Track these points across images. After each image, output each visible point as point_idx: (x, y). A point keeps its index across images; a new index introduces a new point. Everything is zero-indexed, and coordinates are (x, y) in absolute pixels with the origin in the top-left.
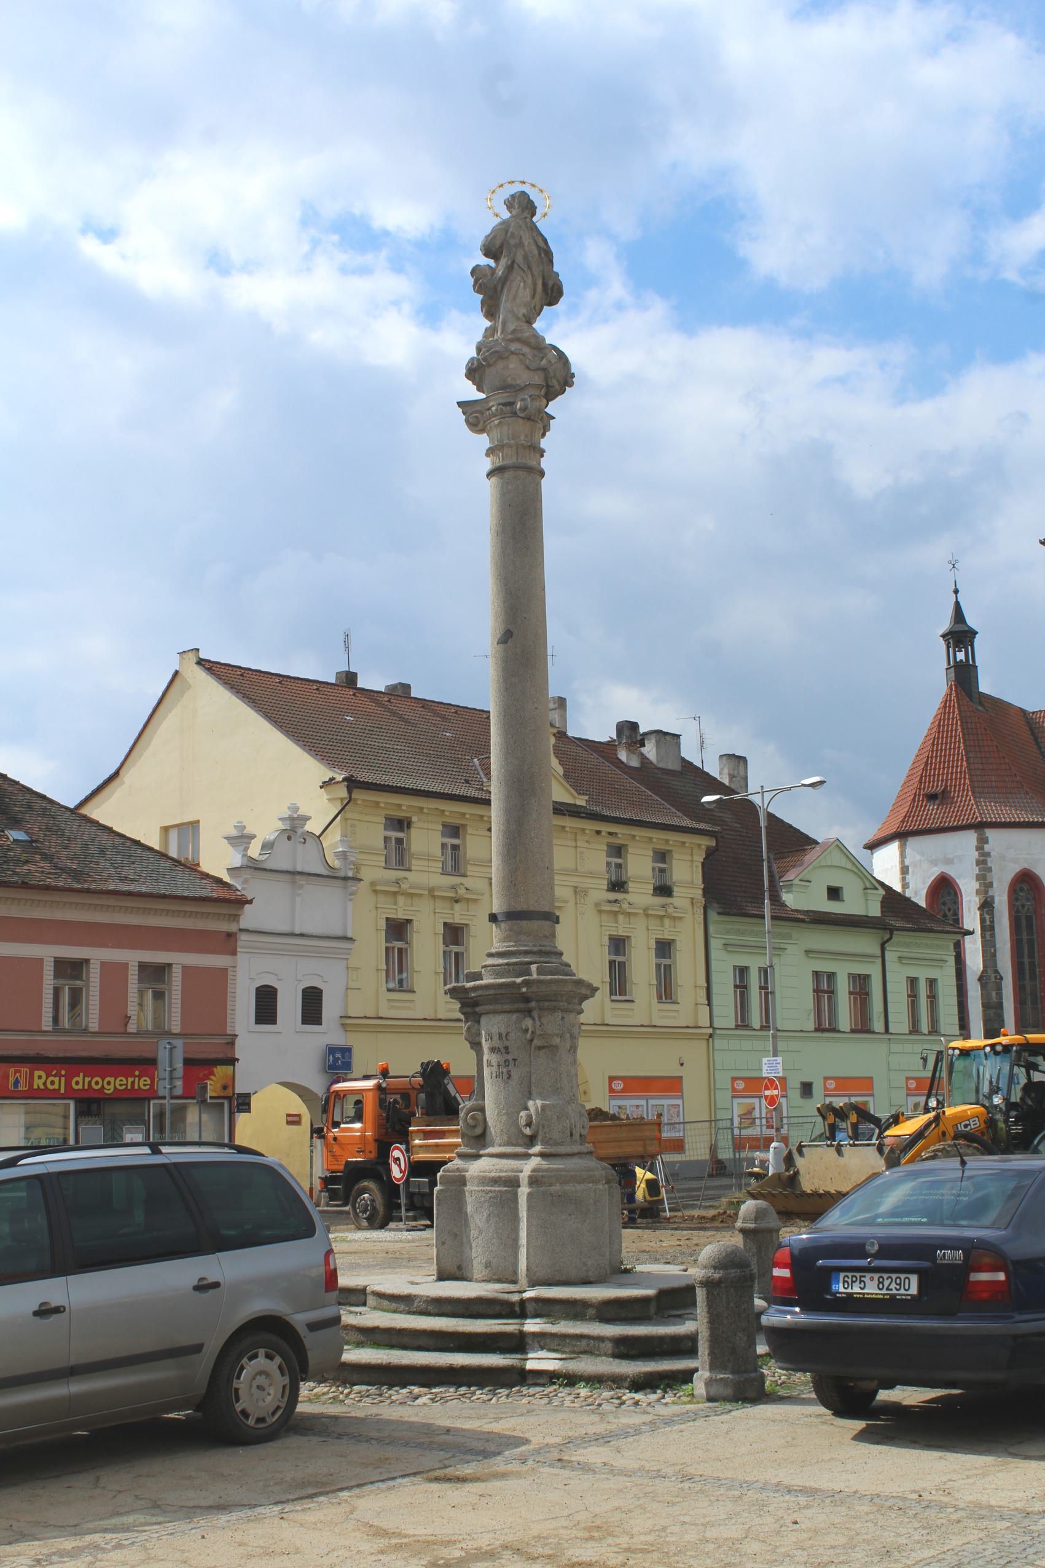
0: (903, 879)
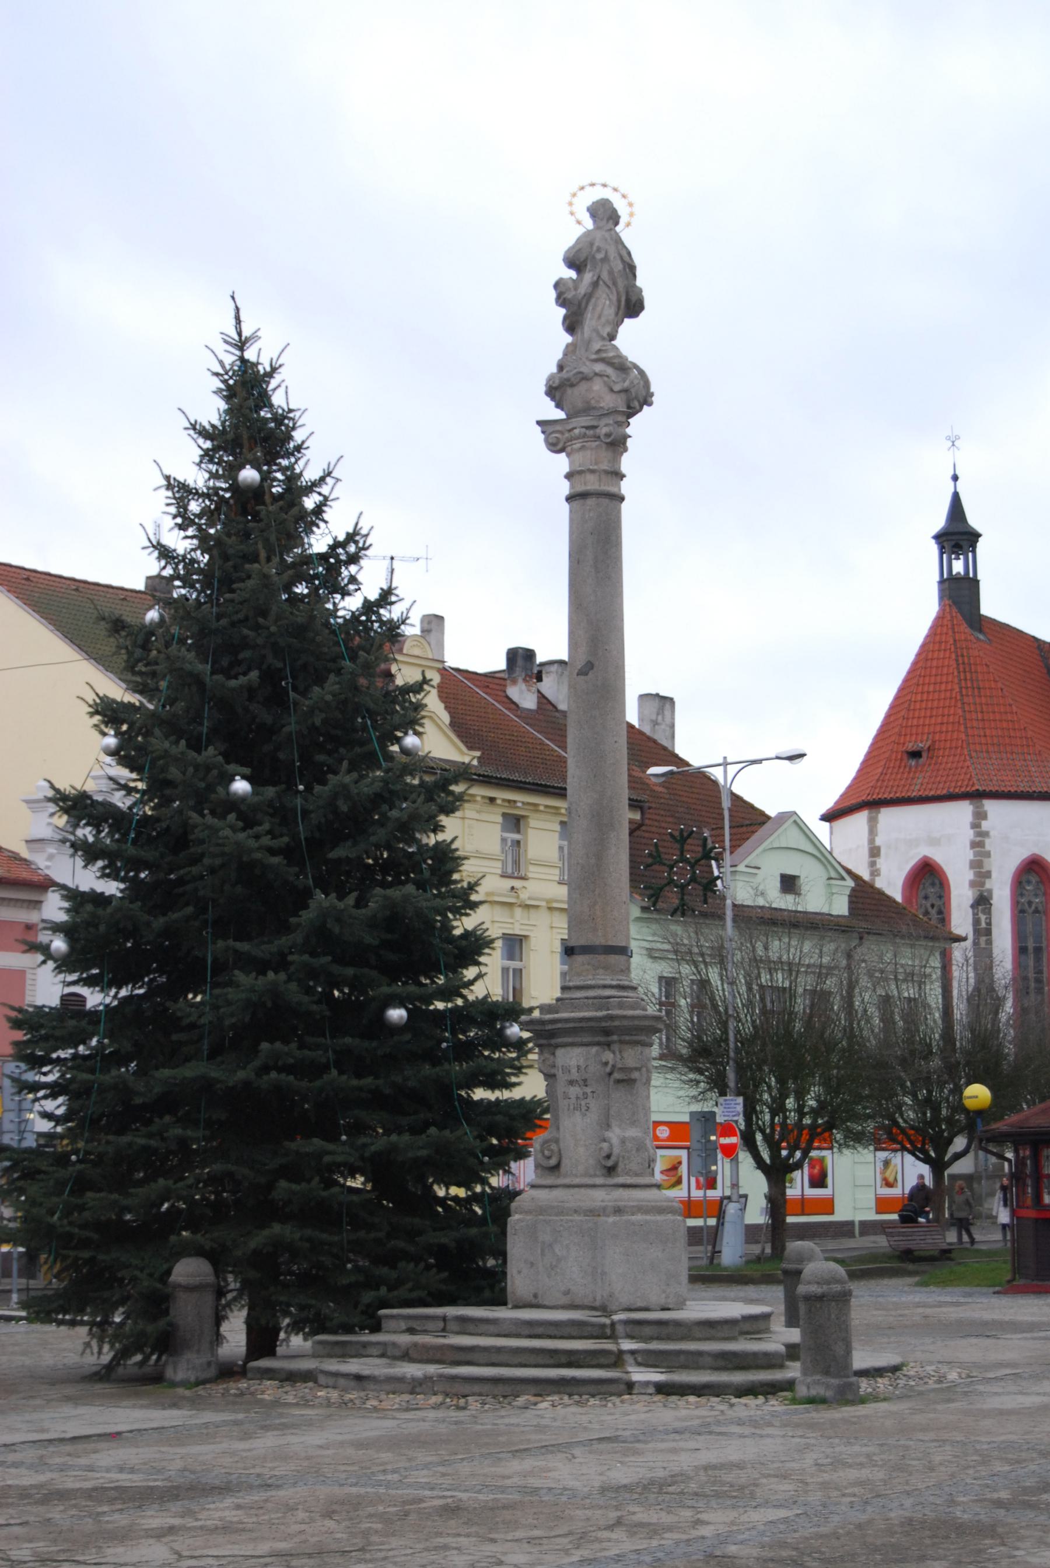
0: (873, 864)
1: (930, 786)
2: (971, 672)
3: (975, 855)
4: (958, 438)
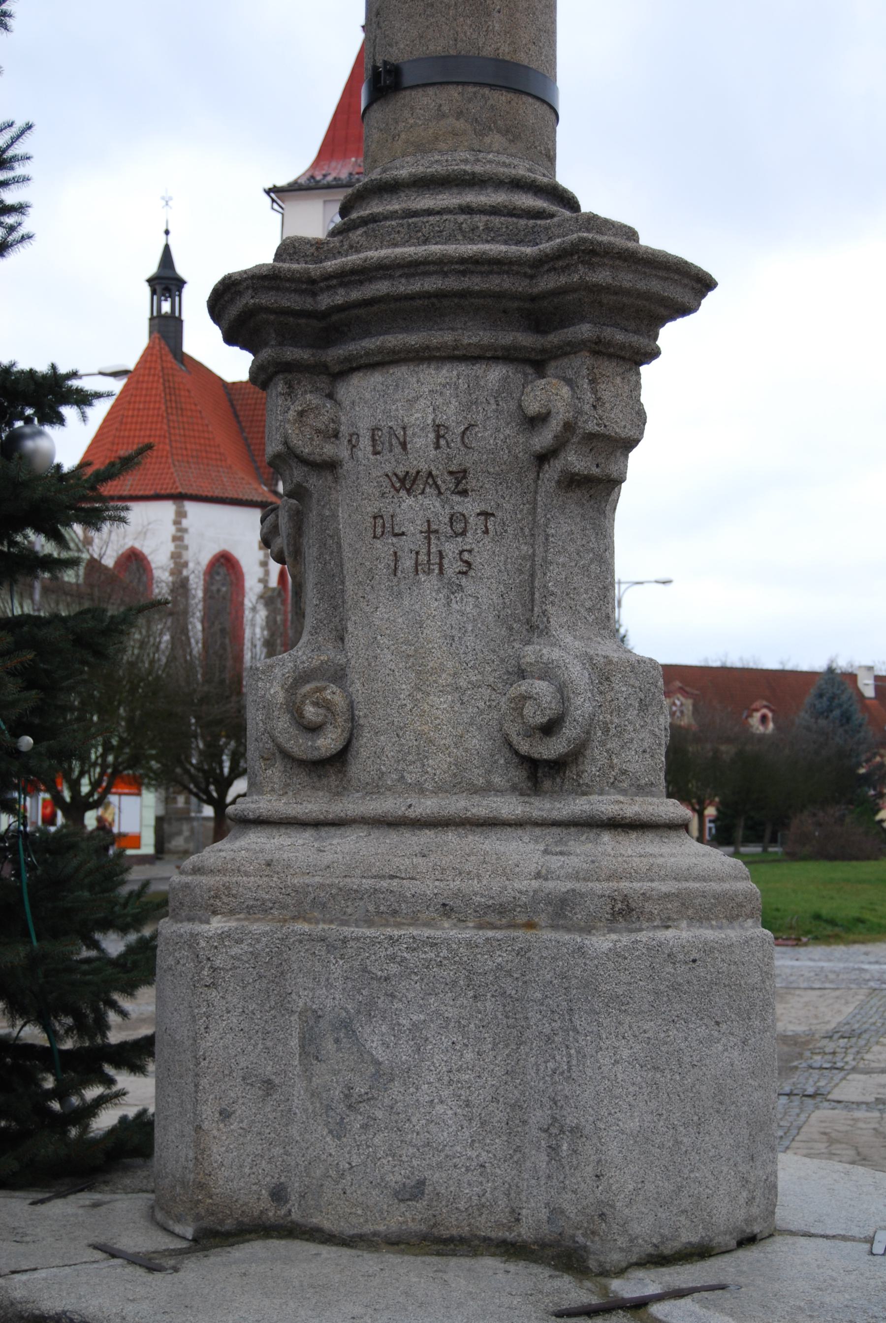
1: (139, 487)
2: (175, 395)
3: (176, 547)
4: (171, 199)
